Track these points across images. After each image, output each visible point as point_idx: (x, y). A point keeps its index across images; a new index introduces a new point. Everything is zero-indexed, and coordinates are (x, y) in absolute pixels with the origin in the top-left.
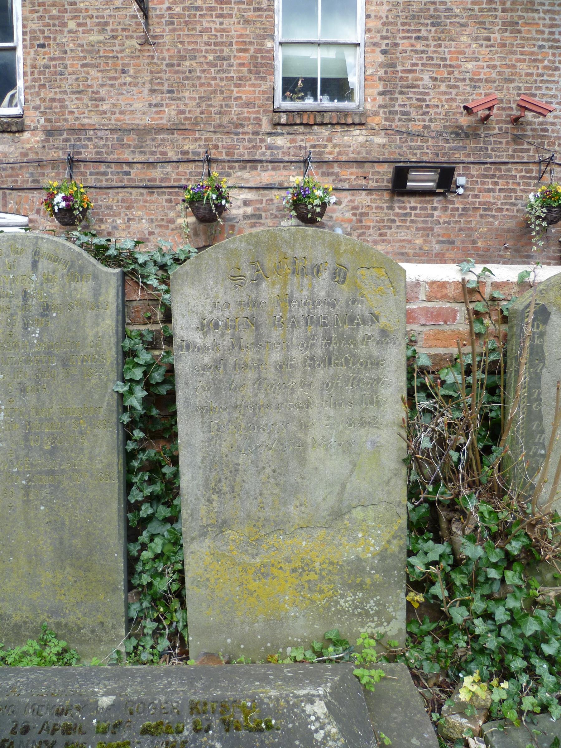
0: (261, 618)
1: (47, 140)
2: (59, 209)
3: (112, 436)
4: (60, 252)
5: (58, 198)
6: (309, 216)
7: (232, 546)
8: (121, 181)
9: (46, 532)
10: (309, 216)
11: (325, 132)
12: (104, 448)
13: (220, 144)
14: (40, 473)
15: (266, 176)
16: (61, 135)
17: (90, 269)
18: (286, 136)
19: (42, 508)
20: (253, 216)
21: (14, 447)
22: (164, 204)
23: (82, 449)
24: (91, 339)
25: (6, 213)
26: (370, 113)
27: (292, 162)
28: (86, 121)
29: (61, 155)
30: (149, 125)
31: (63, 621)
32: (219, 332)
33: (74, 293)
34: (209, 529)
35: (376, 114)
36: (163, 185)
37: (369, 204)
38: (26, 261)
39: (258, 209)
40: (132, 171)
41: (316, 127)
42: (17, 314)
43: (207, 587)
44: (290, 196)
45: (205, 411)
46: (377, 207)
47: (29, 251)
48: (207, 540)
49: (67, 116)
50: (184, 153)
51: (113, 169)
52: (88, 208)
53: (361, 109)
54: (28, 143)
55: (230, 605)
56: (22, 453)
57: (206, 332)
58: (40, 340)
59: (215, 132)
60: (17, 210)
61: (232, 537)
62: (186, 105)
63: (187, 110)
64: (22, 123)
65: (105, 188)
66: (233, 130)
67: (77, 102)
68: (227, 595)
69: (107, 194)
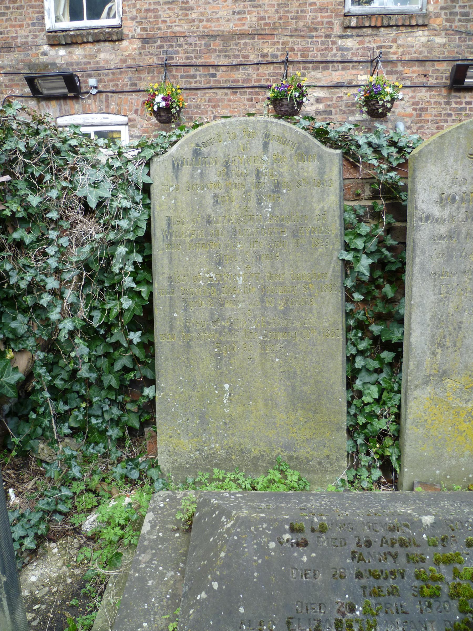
0: (467, 453)
1: (143, 48)
2: (159, 108)
3: (337, 298)
4: (288, 135)
5: (158, 99)
6: (380, 111)
7: (449, 393)
8: (208, 83)
9: (280, 380)
10: (380, 111)
11: (391, 33)
12: (331, 309)
13: (296, 47)
14: (275, 330)
15: (337, 76)
16: (155, 42)
17: (315, 150)
18: (355, 38)
19: (277, 360)
20: (324, 112)
21: (252, 307)
22: (246, 102)
23: (311, 309)
24: (317, 212)
25: (109, 113)
26: (432, 15)
27: (360, 62)
28: (177, 29)
29: (155, 60)
30: (234, 31)
31: (295, 454)
32: (456, 205)
33: (301, 171)
34: (431, 378)
35: (437, 16)
36: (245, 85)
37: (429, 99)
38: (258, 143)
39: (329, 105)
40: (218, 73)
41: (382, 29)
42: (251, 190)
43: (424, 427)
44: (363, 93)
45: (437, 275)
46: (435, 103)
47: (260, 134)
48: (428, 388)
49: (160, 25)
50: (264, 56)
51: (201, 72)
52: (182, 107)
53: (424, 11)
54: (126, 51)
55: (443, 442)
56: (259, 313)
57: (444, 205)
58: (272, 214)
59: (291, 36)
60: (118, 111)
61: (450, 385)
62: (266, 11)
63: (267, 16)
64: (122, 33)
65: (194, 89)
66: (308, 34)
67: (169, 12)
68: (440, 434)
69: (195, 94)
